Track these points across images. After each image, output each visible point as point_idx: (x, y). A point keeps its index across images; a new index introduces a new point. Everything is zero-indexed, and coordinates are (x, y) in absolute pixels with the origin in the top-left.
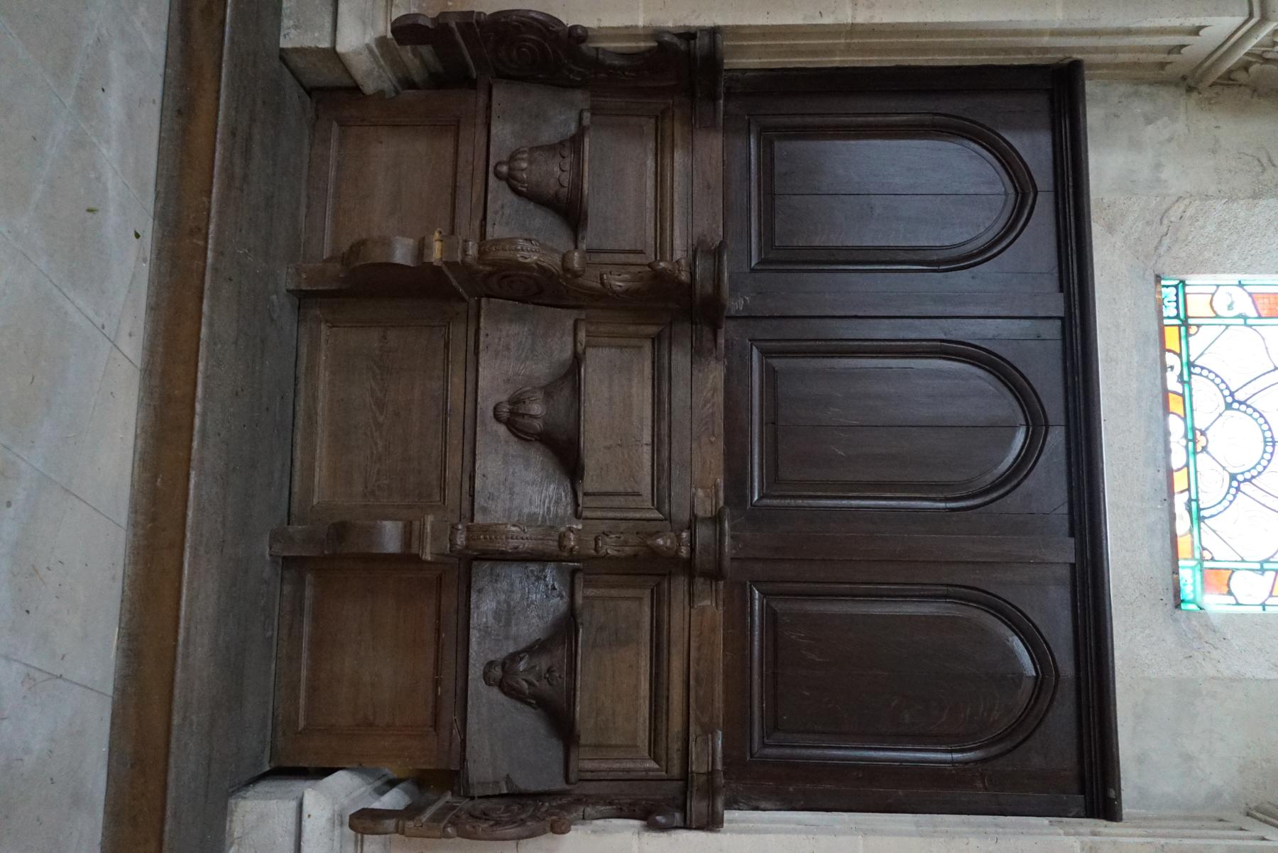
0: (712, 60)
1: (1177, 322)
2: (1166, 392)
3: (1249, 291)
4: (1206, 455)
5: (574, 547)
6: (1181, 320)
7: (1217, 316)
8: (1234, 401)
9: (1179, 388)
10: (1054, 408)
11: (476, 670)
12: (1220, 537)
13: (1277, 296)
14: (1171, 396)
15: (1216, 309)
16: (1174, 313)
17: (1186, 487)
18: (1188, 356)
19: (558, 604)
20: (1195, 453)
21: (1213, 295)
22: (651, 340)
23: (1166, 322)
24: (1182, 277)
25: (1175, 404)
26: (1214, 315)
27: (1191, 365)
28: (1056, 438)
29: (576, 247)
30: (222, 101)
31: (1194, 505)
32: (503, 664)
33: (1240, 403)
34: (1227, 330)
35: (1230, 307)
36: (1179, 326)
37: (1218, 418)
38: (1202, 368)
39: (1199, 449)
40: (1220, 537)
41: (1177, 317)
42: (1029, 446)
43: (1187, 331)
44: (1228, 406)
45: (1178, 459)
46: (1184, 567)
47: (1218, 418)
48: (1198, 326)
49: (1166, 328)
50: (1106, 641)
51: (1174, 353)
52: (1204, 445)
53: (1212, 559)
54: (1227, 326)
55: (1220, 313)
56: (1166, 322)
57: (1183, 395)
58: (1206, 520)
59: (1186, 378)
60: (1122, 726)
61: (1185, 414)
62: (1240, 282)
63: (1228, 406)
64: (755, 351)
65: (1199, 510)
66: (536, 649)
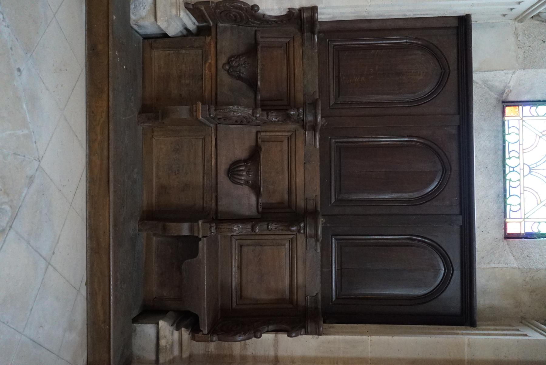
10: (455, 167)
28: (457, 275)
64: (334, 240)
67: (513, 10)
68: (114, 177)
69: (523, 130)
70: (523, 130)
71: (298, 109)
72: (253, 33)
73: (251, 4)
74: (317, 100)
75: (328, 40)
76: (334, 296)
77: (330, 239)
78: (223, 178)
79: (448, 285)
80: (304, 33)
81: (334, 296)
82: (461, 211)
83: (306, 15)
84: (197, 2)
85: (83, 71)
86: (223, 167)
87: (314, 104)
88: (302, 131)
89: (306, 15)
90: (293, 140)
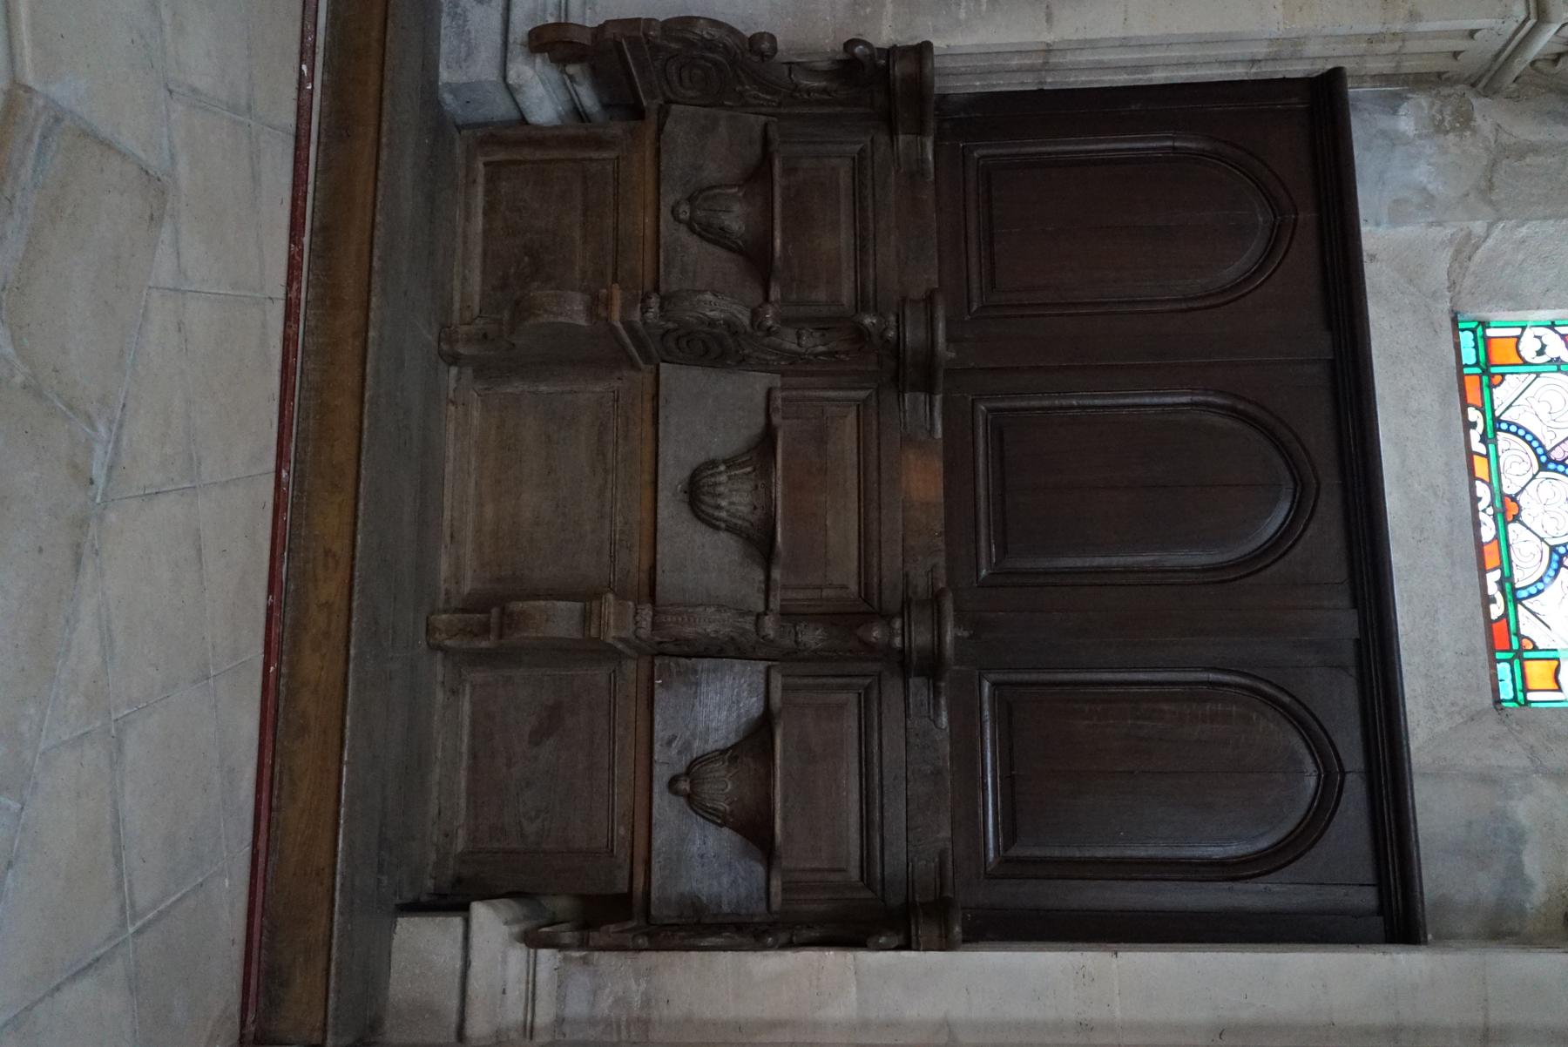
0: (919, 85)
1: (1477, 370)
2: (1470, 454)
3: (1562, 333)
4: (1519, 525)
5: (771, 327)
6: (1477, 326)
7: (1526, 363)
8: (1550, 460)
9: (1481, 448)
10: (1352, 756)
11: (662, 774)
12: (1543, 622)
13: (1567, 65)
14: (1476, 458)
15: (1522, 354)
16: (1473, 361)
17: (1498, 564)
18: (1493, 411)
19: (752, 706)
20: (1506, 523)
21: (1518, 338)
22: (857, 695)
23: (1466, 371)
24: (1484, 315)
25: (1480, 466)
26: (1521, 362)
27: (1497, 420)
28: (1355, 790)
29: (767, 299)
30: (350, 687)
31: (1508, 586)
32: (688, 773)
33: (1557, 462)
34: (1538, 379)
35: (1541, 352)
36: (1480, 376)
37: (1539, 537)
38: (1510, 424)
39: (1510, 519)
40: (1543, 622)
41: (1477, 364)
42: (1322, 795)
43: (1490, 380)
44: (1543, 467)
45: (1487, 533)
46: (1463, 330)
47: (1539, 537)
48: (1503, 375)
49: (1466, 378)
50: (1403, 765)
51: (1483, 481)
52: (1515, 513)
53: (1535, 648)
54: (1538, 374)
55: (1528, 359)
56: (1466, 371)
57: (1487, 456)
58: (1524, 602)
59: (1490, 435)
60: (1409, 664)
61: (1483, 404)
62: (1553, 323)
63: (1543, 467)
64: (986, 686)
65: (1514, 590)
66: (731, 754)
67: (1477, 35)
68: (342, 885)
69: (1529, 385)
70: (1529, 385)
71: (889, 624)
72: (760, 398)
73: (748, 34)
74: (942, 590)
75: (970, 398)
76: (991, 855)
77: (977, 682)
78: (671, 510)
79: (1327, 825)
80: (897, 134)
81: (991, 855)
82: (1381, 905)
83: (899, 69)
84: (607, 22)
85: (284, 204)
86: (673, 476)
87: (935, 600)
88: (898, 683)
89: (899, 69)
90: (875, 693)
